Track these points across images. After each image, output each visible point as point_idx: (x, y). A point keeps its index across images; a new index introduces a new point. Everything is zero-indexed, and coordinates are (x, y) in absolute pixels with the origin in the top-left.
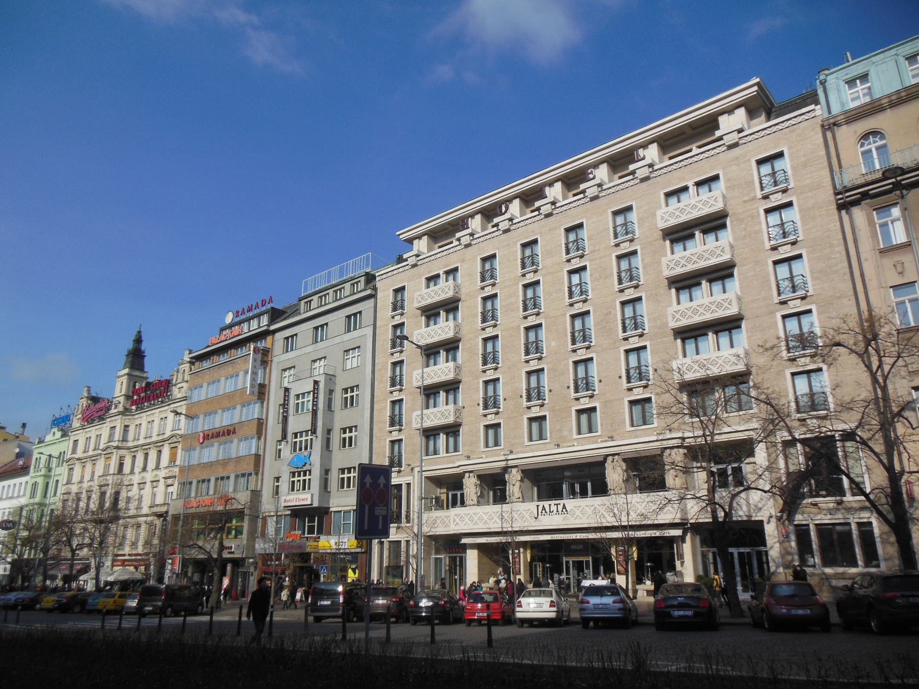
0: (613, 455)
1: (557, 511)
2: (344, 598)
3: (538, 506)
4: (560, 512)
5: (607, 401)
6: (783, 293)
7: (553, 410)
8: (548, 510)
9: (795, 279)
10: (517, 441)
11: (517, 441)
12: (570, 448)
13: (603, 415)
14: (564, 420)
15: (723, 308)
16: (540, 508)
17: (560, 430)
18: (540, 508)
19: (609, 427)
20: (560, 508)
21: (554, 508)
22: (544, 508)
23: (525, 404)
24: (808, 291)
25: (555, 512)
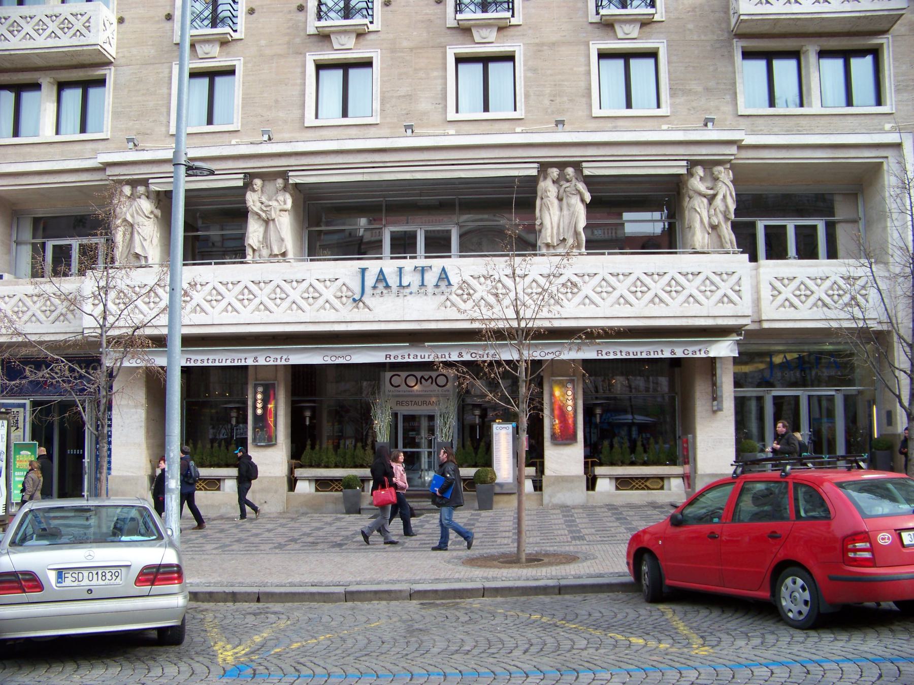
0: (562, 166)
1: (423, 285)
2: (851, 558)
3: (363, 271)
4: (430, 288)
5: (543, 44)
6: (223, 20)
7: (393, 50)
8: (393, 281)
9: (220, 9)
10: (281, 114)
11: (281, 114)
12: (438, 138)
13: (529, 74)
14: (421, 74)
15: (72, 31)
16: (370, 280)
17: (410, 97)
18: (370, 280)
19: (547, 102)
20: (431, 278)
21: (410, 278)
22: (381, 277)
23: (313, 25)
24: (235, 31)
25: (415, 287)
